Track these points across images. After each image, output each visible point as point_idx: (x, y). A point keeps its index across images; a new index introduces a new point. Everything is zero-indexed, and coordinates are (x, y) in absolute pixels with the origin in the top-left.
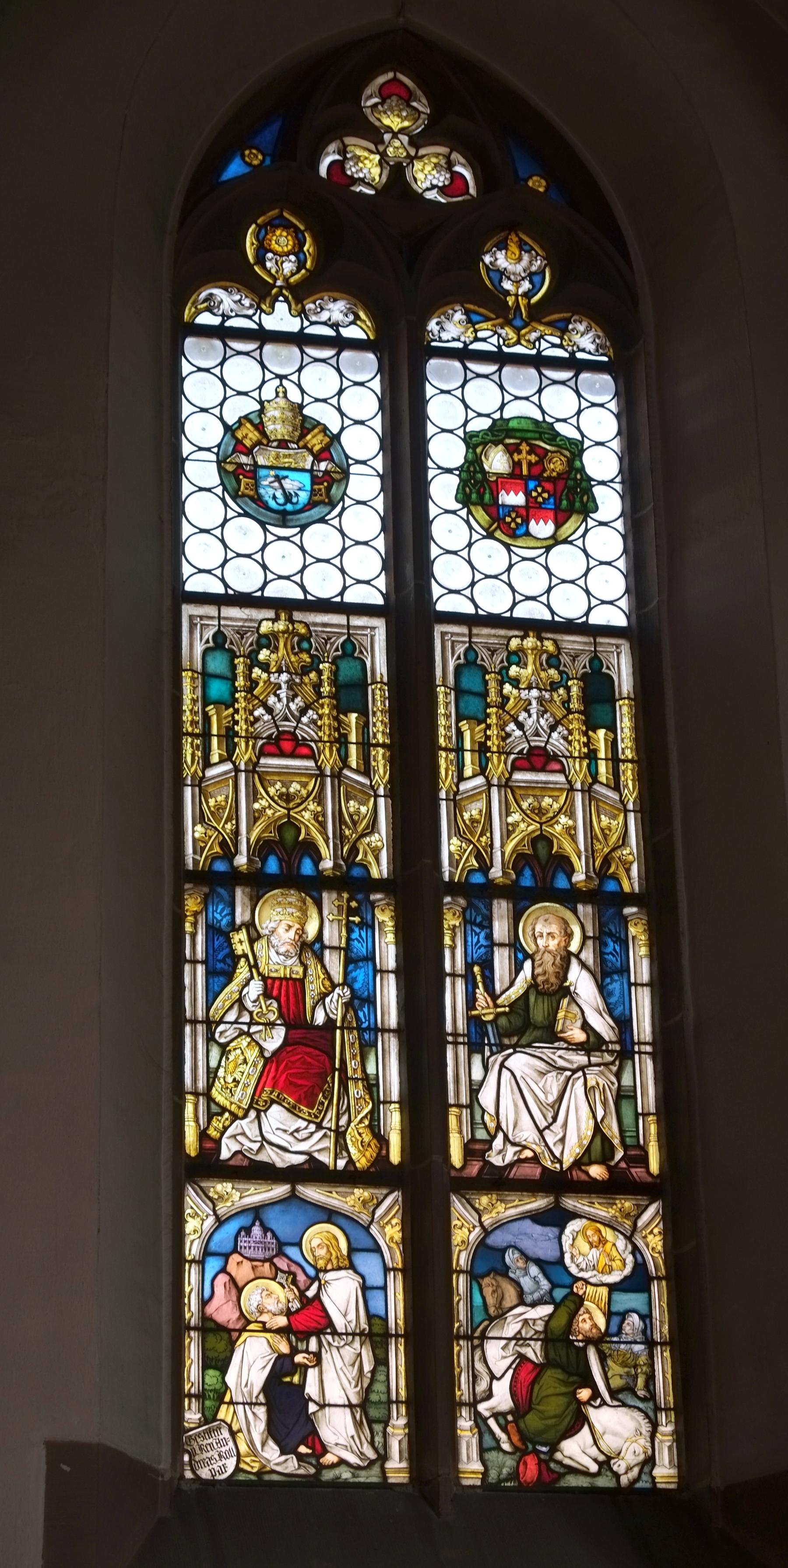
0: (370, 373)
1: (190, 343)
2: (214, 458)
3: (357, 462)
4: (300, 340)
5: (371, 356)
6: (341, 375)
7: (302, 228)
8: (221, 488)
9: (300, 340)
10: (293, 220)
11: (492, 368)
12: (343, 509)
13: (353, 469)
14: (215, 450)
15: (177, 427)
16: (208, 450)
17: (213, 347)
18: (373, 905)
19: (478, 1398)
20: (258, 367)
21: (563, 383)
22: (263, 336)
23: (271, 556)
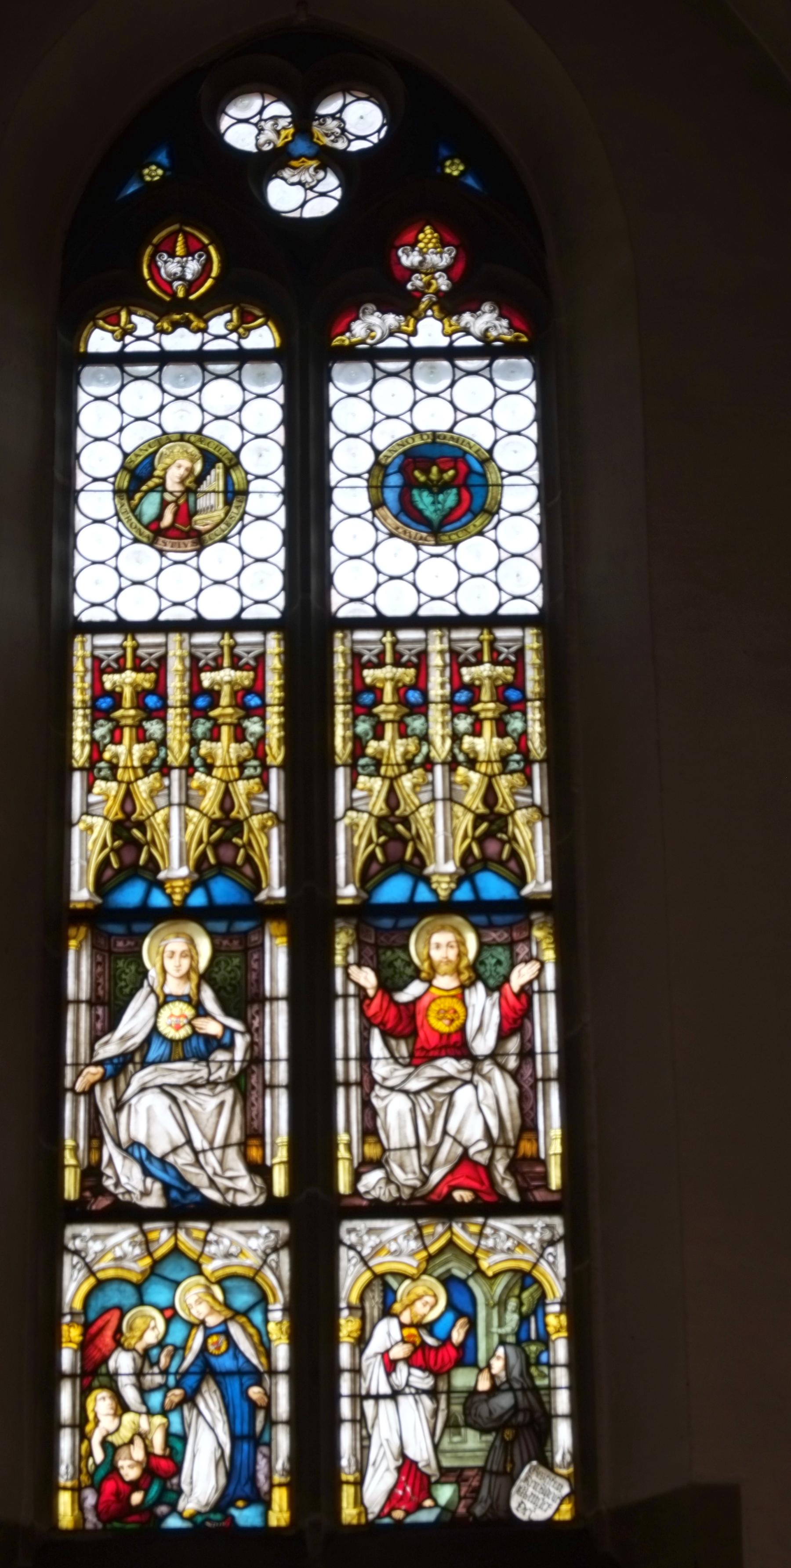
0: (196, 382)
1: (338, 369)
2: (365, 484)
3: (511, 474)
4: (451, 353)
5: (525, 362)
6: (244, 389)
7: (206, 241)
8: (115, 518)
9: (451, 353)
10: (163, 233)
11: (404, 364)
12: (499, 521)
13: (253, 487)
14: (366, 476)
15: (71, 457)
16: (358, 476)
17: (520, 368)
18: (531, 925)
19: (83, 1485)
20: (409, 388)
21: (226, 376)
22: (413, 355)
23: (165, 583)
